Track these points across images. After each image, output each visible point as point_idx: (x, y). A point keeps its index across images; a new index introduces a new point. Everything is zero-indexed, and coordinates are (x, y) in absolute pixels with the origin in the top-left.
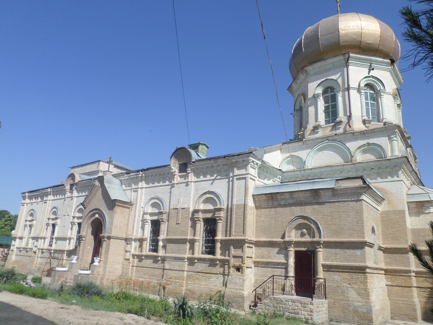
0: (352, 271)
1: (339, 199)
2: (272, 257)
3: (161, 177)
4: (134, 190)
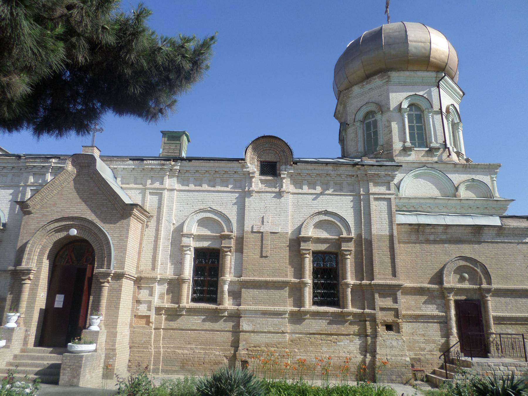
0: (526, 323)
1: (505, 240)
2: (423, 308)
3: (218, 176)
4: (151, 191)
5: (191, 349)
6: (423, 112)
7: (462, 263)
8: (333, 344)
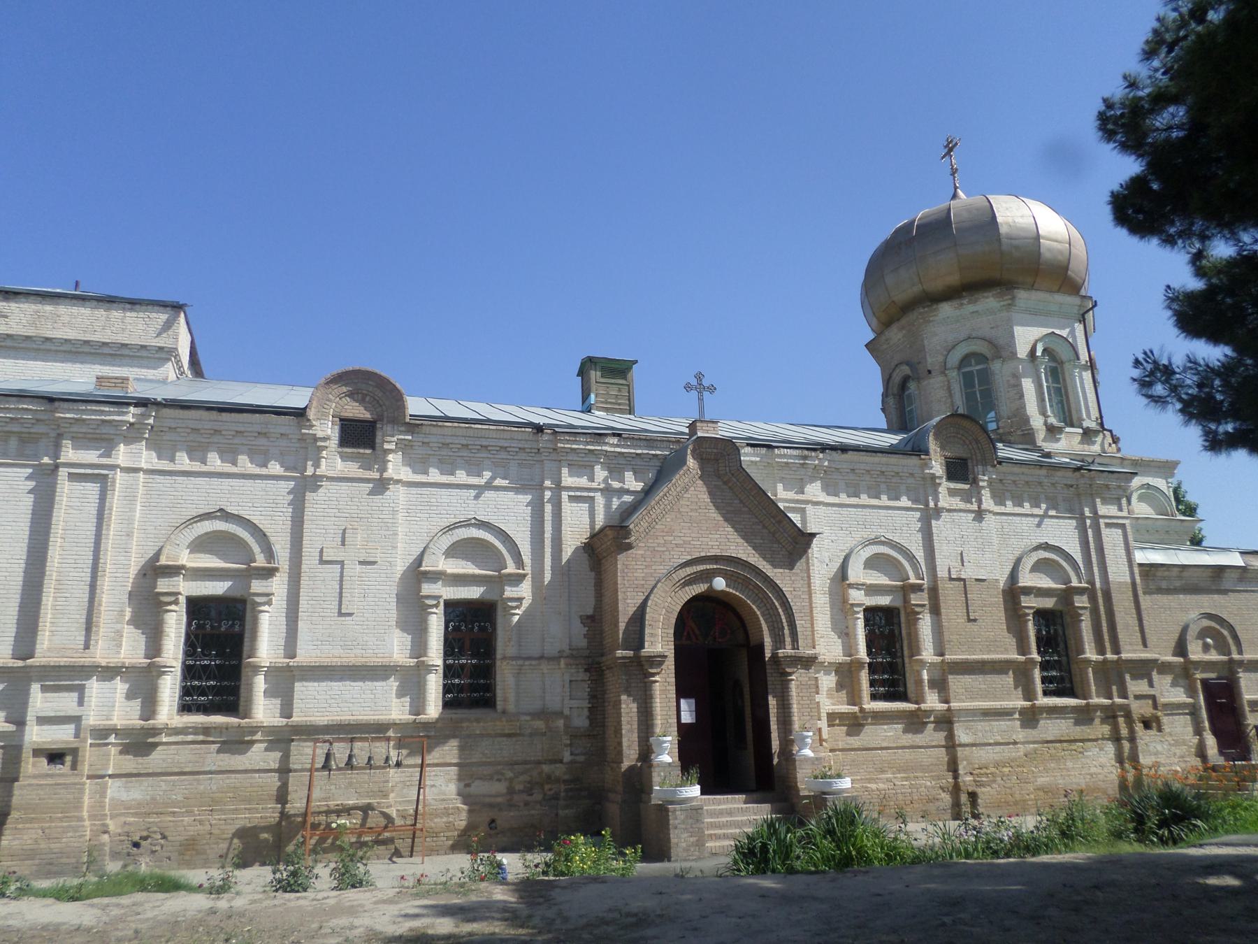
5: (889, 780)
6: (1062, 363)
7: (1206, 623)
8: (1080, 755)
